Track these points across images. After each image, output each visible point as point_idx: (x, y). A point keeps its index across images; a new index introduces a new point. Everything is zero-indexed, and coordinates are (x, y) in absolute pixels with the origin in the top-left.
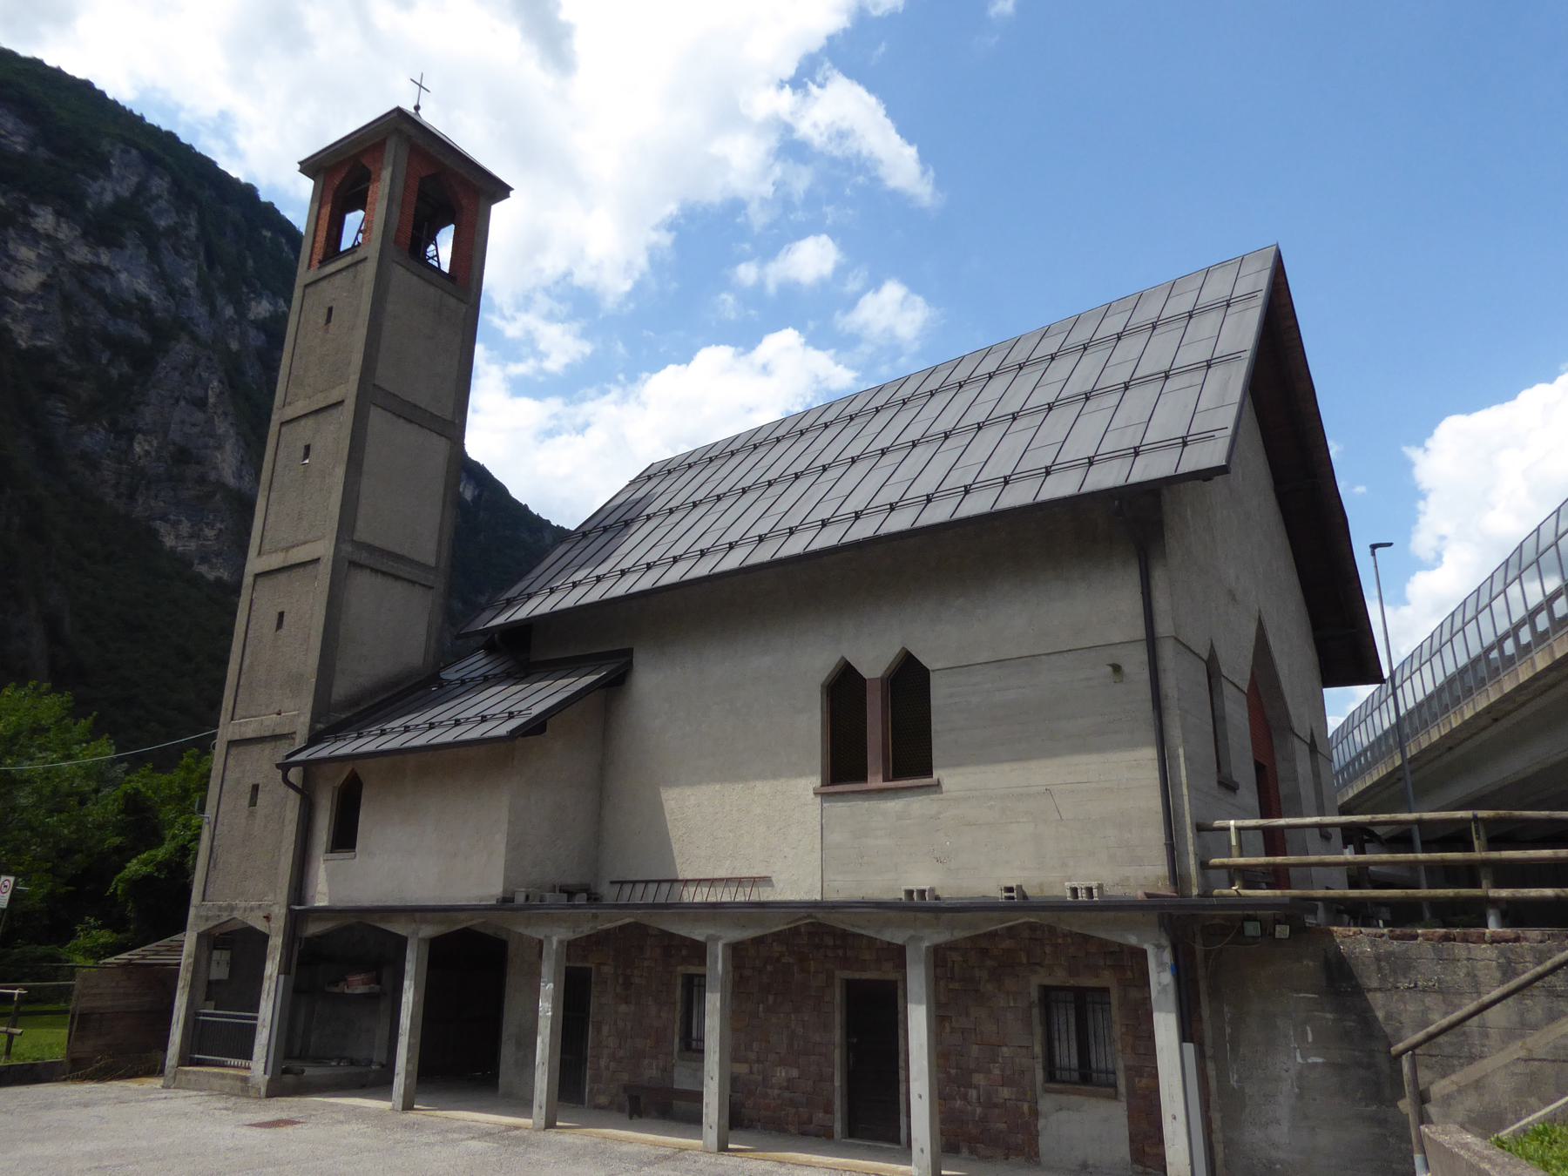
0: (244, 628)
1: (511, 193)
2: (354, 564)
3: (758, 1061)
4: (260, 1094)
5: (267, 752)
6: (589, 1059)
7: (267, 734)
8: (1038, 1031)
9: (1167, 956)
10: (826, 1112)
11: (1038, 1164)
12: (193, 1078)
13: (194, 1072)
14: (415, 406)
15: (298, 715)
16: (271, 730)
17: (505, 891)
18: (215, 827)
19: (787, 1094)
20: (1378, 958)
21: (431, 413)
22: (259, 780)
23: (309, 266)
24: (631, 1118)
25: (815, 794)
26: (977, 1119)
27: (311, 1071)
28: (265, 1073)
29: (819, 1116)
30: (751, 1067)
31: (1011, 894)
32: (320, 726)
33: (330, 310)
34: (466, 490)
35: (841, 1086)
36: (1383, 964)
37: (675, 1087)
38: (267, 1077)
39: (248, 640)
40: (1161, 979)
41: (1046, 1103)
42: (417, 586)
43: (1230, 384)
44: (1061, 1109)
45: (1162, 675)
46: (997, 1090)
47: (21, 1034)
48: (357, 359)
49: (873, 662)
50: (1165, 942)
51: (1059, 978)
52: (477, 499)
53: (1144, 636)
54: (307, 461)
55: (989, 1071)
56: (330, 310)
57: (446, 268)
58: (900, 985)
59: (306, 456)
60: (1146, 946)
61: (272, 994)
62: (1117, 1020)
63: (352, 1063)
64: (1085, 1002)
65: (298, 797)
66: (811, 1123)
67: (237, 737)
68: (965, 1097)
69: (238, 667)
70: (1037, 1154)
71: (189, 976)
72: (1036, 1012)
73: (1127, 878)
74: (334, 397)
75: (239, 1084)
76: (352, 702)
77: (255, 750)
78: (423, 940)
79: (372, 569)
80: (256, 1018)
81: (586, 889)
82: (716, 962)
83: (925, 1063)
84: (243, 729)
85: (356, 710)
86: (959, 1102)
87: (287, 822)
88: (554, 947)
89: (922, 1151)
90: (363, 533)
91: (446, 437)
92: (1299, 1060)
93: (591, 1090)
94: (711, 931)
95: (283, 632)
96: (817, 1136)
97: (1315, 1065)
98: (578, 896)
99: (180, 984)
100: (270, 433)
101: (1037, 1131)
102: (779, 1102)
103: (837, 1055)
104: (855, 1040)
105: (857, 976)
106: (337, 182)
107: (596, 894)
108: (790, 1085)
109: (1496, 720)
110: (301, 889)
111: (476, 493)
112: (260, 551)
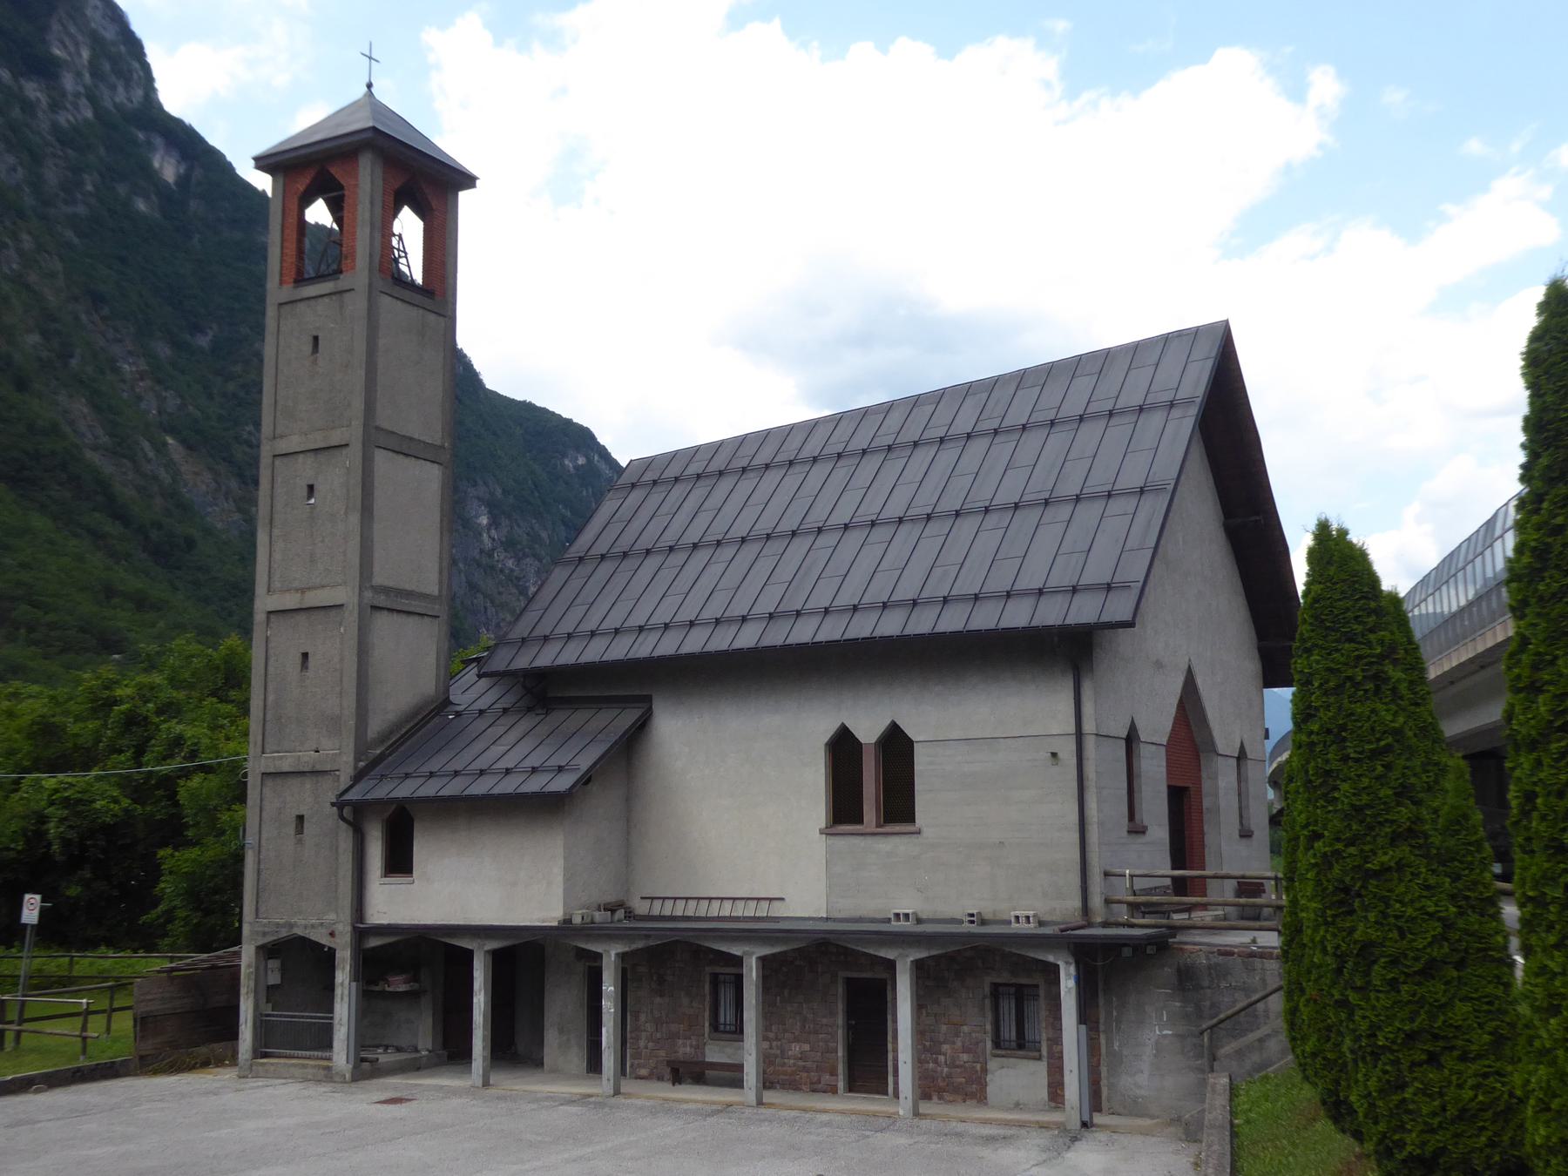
0: (263, 666)
1: (478, 182)
2: (375, 608)
3: (777, 1039)
4: (345, 1078)
5: (308, 786)
6: (628, 1041)
7: (306, 769)
8: (989, 1016)
9: (1072, 969)
10: (832, 1075)
11: (986, 1104)
12: (272, 1068)
13: (272, 1064)
14: (411, 439)
15: (340, 754)
16: (310, 766)
17: (565, 914)
19: (801, 1063)
20: (1209, 967)
21: (424, 442)
22: (303, 810)
23: (281, 283)
24: (674, 1085)
25: (821, 833)
26: (944, 1075)
27: (384, 1058)
28: (348, 1062)
29: (826, 1078)
30: (771, 1044)
31: (972, 919)
32: (362, 764)
33: (316, 339)
34: (166, 165)
35: (844, 1056)
36: (1212, 971)
37: (707, 1060)
38: (351, 1066)
40: (1068, 984)
41: (992, 1064)
43: (1184, 424)
44: (1003, 1067)
45: (1085, 762)
46: (958, 1056)
47: (97, 1037)
48: (358, 404)
49: (868, 731)
50: (1071, 960)
51: (1005, 978)
52: (183, 181)
53: (1074, 732)
54: (312, 501)
55: (954, 1043)
56: (316, 339)
57: (418, 277)
58: (889, 982)
60: (1059, 963)
61: (346, 999)
62: (1041, 1009)
63: (399, 1050)
64: (1022, 995)
66: (820, 1083)
68: (936, 1062)
69: (261, 703)
70: (986, 1098)
71: (252, 984)
72: (988, 1002)
73: (1055, 909)
75: (322, 1072)
76: (382, 738)
77: (294, 783)
78: (488, 952)
80: (332, 1018)
81: (621, 905)
82: (751, 971)
83: (910, 1042)
84: (278, 763)
86: (931, 1065)
87: (341, 851)
88: (613, 959)
89: (906, 1098)
90: (379, 579)
91: (438, 463)
92: (1158, 1032)
93: (632, 1066)
94: (747, 949)
95: (310, 673)
96: (824, 1092)
97: (1166, 1036)
98: (618, 912)
99: (243, 991)
101: (986, 1082)
102: (794, 1069)
103: (840, 1032)
104: (853, 1022)
105: (855, 975)
107: (630, 908)
108: (803, 1056)
109: (1482, 667)
110: (361, 910)
111: (182, 171)
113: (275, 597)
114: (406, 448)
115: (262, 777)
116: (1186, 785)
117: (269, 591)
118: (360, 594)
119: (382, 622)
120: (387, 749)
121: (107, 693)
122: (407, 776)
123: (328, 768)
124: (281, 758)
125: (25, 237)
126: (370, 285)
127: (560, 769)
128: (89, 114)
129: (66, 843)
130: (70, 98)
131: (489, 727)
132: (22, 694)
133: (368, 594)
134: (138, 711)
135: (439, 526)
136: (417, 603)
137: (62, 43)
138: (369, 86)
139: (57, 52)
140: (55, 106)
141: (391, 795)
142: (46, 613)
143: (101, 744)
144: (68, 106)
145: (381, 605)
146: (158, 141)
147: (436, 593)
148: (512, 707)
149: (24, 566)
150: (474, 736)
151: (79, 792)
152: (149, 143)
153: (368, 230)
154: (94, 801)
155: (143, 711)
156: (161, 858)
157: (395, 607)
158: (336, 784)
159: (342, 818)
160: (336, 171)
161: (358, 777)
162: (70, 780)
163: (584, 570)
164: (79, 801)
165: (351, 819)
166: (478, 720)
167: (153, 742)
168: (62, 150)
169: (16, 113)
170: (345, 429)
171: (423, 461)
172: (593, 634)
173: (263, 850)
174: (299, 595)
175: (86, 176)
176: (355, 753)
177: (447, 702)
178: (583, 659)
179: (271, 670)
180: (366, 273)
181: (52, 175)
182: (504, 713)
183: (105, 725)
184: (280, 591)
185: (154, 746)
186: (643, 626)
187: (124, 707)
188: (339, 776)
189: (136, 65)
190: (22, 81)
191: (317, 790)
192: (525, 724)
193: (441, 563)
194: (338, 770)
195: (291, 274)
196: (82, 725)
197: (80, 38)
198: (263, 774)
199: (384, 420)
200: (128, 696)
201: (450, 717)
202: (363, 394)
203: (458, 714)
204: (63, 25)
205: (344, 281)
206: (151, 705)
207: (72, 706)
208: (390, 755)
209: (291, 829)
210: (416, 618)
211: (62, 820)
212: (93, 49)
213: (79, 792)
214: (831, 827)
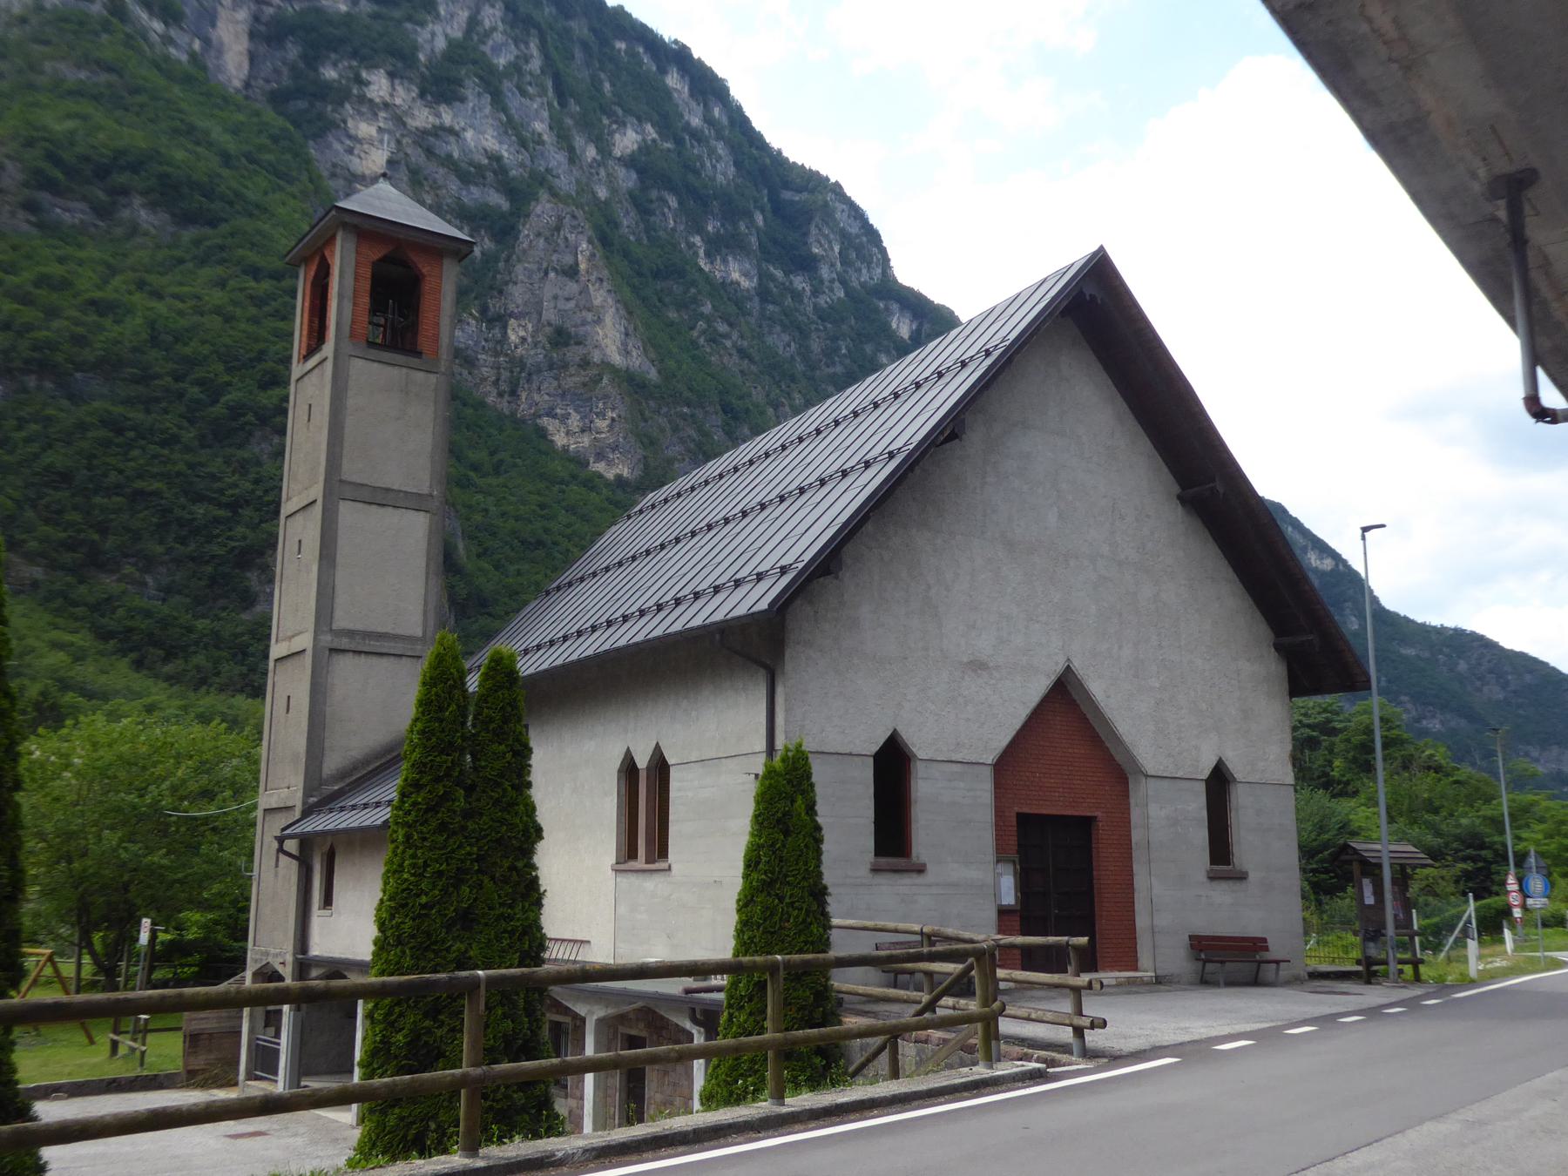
21: (406, 492)
23: (299, 362)
32: (313, 800)
56: (310, 405)
76: (342, 775)
79: (354, 652)
85: (348, 781)
90: (342, 621)
95: (289, 715)
114: (381, 498)
116: (1093, 814)
119: (344, 664)
125: (797, 395)
128: (842, 295)
130: (826, 283)
137: (819, 242)
140: (816, 292)
144: (827, 291)
145: (342, 648)
146: (895, 306)
147: (419, 633)
152: (887, 309)
157: (360, 649)
161: (307, 812)
169: (788, 301)
175: (841, 343)
181: (816, 345)
189: (875, 250)
190: (792, 277)
197: (832, 236)
199: (352, 470)
210: (392, 659)
214: (625, 862)
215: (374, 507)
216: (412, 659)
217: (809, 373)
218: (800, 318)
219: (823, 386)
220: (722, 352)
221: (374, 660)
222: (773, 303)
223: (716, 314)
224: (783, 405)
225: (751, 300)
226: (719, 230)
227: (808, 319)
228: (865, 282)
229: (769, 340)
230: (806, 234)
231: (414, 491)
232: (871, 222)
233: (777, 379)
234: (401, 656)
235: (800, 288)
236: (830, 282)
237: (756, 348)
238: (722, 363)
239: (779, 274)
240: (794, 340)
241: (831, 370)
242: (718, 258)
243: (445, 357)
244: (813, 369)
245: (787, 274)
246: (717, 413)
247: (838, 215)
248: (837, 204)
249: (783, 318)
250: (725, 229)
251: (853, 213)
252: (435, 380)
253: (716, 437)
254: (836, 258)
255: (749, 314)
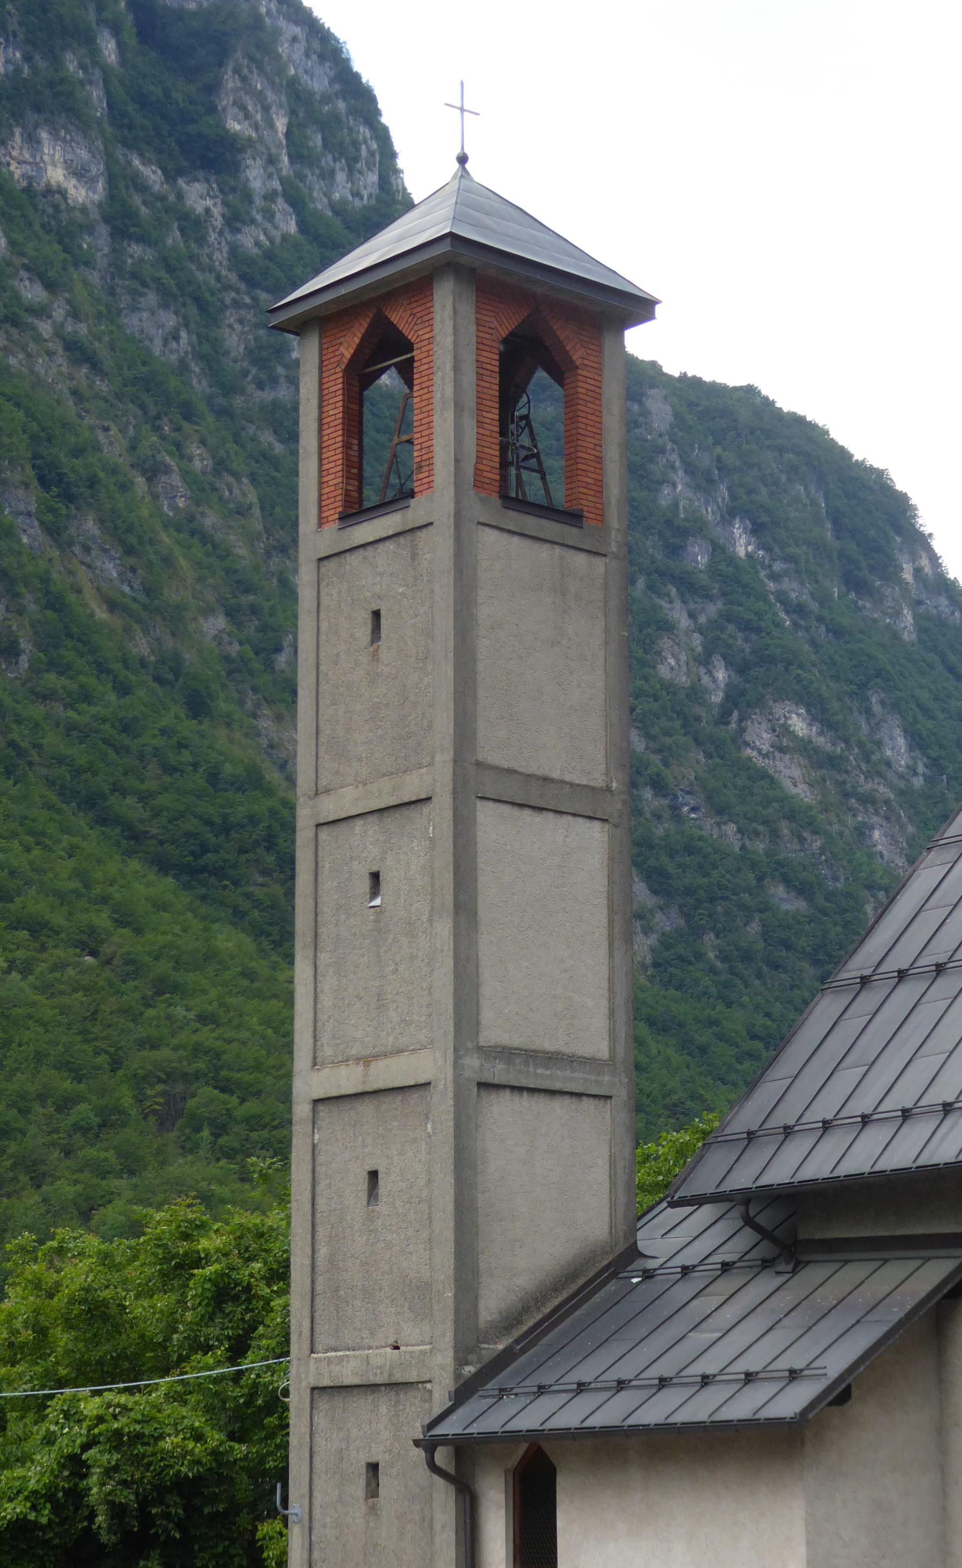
0: (308, 1195)
1: (658, 308)
2: (484, 1086)
5: (383, 1409)
7: (379, 1380)
14: (546, 779)
18: (310, 1529)
21: (572, 785)
23: (321, 522)
32: (469, 1370)
33: (377, 614)
39: (318, 1215)
42: (584, 1098)
48: (444, 723)
54: (377, 902)
56: (377, 614)
59: (375, 890)
65: (452, 1489)
67: (326, 1382)
69: (308, 1262)
74: (411, 788)
76: (508, 1322)
77: (361, 1404)
79: (513, 1088)
84: (336, 1369)
85: (517, 1333)
87: (438, 1526)
95: (382, 1207)
100: (299, 842)
106: (347, 353)
112: (315, 1058)
113: (326, 1071)
115: (312, 1394)
117: (315, 1064)
118: (455, 1062)
120: (517, 1342)
121: (183, 1247)
122: (542, 1390)
123: (412, 1376)
124: (341, 1359)
125: (196, 451)
126: (458, 516)
127: (794, 1375)
128: (292, 227)
129: (117, 1511)
130: (258, 202)
131: (693, 1298)
132: (69, 1250)
133: (473, 1062)
134: (234, 1275)
135: (605, 932)
136: (568, 1073)
137: (243, 108)
138: (463, 160)
139: (234, 126)
140: (234, 221)
141: (510, 1427)
142: (243, 1101)
143: (175, 1336)
144: (259, 217)
145: (496, 1081)
148: (740, 1259)
149: (203, 1019)
150: (666, 1314)
151: (137, 1422)
153: (450, 415)
154: (161, 1437)
155: (243, 1275)
156: (264, 1539)
158: (427, 1406)
159: (433, 1466)
160: (399, 317)
162: (123, 1399)
163: (868, 1000)
164: (137, 1437)
165: (451, 1470)
166: (680, 1283)
167: (261, 1329)
168: (249, 294)
169: (174, 238)
170: (424, 770)
171: (570, 818)
172: (866, 1120)
173: (316, 1524)
174: (361, 1068)
176: (457, 1349)
177: (633, 1253)
178: (844, 1169)
179: (321, 1202)
180: (450, 492)
182: (723, 1273)
183: (182, 1302)
184: (333, 1062)
185: (262, 1336)
186: (951, 1104)
187: (209, 1270)
188: (430, 1392)
190: (181, 182)
191: (396, 1415)
192: (766, 1283)
193: (611, 1000)
194: (430, 1381)
195: (335, 506)
196: (146, 1303)
197: (270, 96)
198: (313, 1389)
200: (218, 1250)
201: (635, 1280)
202: (452, 706)
203: (648, 1275)
204: (244, 79)
205: (417, 511)
206: (257, 1266)
207: (132, 1272)
208: (524, 1351)
209: (358, 1488)
210: (567, 1100)
211: (110, 1471)
212: (293, 113)
213: (137, 1422)
215: (527, 812)
216: (596, 1102)
217: (221, 401)
218: (200, 276)
219: (251, 430)
220: (32, 347)
221: (540, 1104)
222: (141, 239)
223: (17, 260)
224: (167, 470)
225: (89, 229)
226: (18, 70)
227: (218, 278)
228: (343, 201)
229: (133, 322)
230: (213, 88)
231: (584, 782)
232: (357, 66)
233: (153, 410)
234: (579, 1095)
235: (199, 209)
236: (265, 198)
237: (106, 338)
238: (32, 372)
239: (153, 175)
240: (187, 326)
241: (267, 396)
242: (18, 131)
243: (615, 524)
244: (228, 390)
245: (170, 177)
246: (27, 486)
247: (283, 49)
248: (282, 23)
249: (163, 274)
250: (34, 68)
251: (316, 45)
252: (602, 569)
253: (25, 540)
254: (279, 145)
255: (87, 264)
